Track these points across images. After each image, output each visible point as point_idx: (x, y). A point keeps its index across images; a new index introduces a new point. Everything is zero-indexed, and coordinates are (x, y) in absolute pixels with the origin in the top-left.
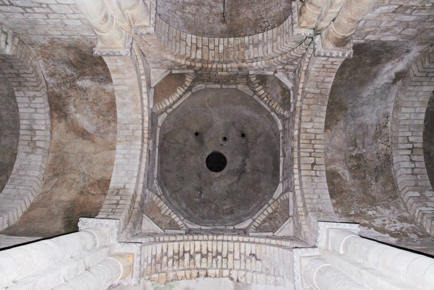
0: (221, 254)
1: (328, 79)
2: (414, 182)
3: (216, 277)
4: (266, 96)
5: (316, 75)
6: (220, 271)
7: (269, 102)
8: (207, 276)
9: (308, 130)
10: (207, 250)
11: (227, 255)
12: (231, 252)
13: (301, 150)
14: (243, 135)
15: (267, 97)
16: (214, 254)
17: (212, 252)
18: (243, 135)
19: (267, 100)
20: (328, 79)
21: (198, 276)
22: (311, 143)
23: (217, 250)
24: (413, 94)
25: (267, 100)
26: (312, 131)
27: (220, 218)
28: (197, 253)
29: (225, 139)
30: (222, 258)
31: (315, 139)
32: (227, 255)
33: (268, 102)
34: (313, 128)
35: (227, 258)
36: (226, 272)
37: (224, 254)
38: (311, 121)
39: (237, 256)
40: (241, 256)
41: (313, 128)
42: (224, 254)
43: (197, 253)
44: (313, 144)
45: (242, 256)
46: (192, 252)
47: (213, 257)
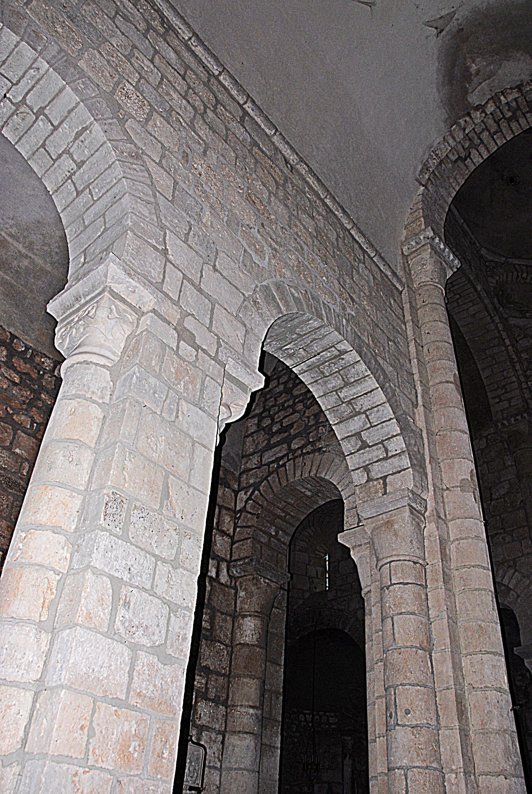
0: (509, 120)
1: (487, 373)
4: (526, 279)
5: (505, 372)
11: (499, 126)
12: (496, 133)
13: (467, 282)
14: (512, 180)
15: (523, 278)
16: (519, 113)
17: (524, 114)
19: (522, 275)
20: (487, 373)
22: (459, 294)
23: (518, 121)
25: (522, 275)
26: (465, 307)
30: (504, 117)
31: (457, 301)
32: (499, 126)
33: (520, 274)
34: (467, 309)
35: (497, 122)
36: (490, 108)
37: (504, 124)
38: (474, 315)
39: (485, 135)
40: (479, 141)
41: (467, 309)
42: (504, 124)
44: (455, 295)
45: (477, 141)
47: (519, 108)
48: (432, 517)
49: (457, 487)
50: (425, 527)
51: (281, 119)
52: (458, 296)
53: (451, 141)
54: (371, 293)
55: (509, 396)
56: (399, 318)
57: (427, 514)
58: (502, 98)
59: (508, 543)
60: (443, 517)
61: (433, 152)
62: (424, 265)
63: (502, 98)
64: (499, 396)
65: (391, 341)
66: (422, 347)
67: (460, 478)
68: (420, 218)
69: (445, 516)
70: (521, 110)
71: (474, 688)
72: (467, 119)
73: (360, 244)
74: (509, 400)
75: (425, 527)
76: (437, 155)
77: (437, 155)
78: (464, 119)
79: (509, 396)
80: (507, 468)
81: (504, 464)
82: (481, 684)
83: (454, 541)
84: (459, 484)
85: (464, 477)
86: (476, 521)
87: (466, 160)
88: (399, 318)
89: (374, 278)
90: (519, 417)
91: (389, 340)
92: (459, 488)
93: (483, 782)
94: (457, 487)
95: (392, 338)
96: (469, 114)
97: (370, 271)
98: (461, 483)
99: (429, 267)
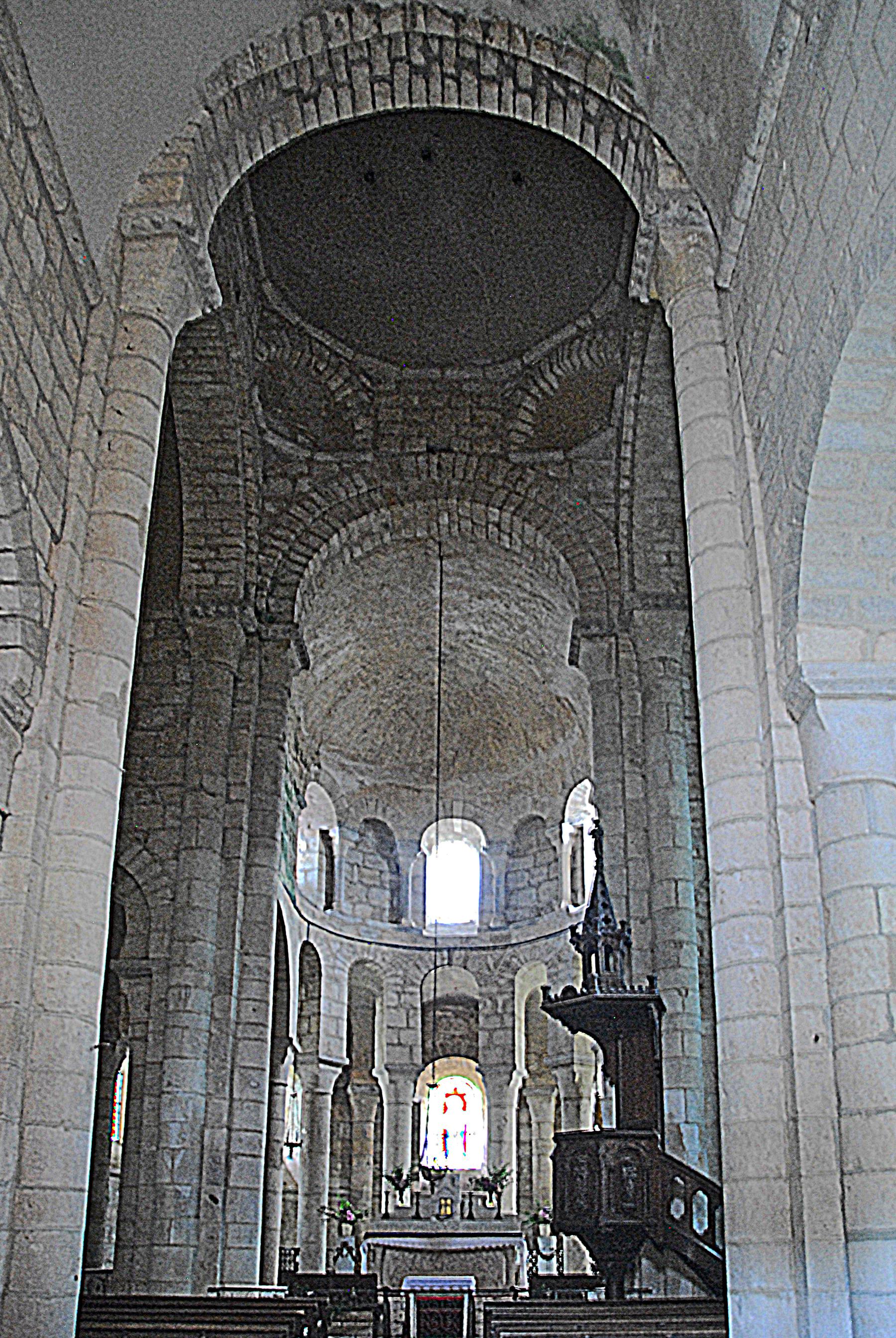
0: (415, 69)
2: (257, 861)
3: (425, 8)
6: (414, 25)
7: (310, 360)
8: (459, 20)
9: (210, 378)
10: (459, 84)
14: (370, 176)
15: (317, 370)
17: (444, 75)
18: (370, 176)
19: (316, 363)
21: (486, 26)
22: (195, 350)
24: (575, 1328)
27: (399, 466)
28: (491, 80)
29: (427, 156)
36: (393, 26)
37: (403, 71)
43: (491, 80)
46: (509, 84)
48: (37, 741)
49: (93, 702)
50: (20, 753)
51: (455, 703)
52: (191, 352)
53: (296, 45)
54: (33, 289)
55: (220, 566)
56: (73, 361)
57: (27, 733)
58: (421, 18)
59: (145, 804)
60: (56, 746)
61: (252, 46)
62: (153, 274)
63: (421, 18)
64: (202, 562)
65: (45, 400)
66: (100, 433)
67: (102, 689)
68: (177, 174)
69: (60, 744)
70: (441, 64)
71: (45, 1010)
72: (344, 19)
73: (40, 170)
74: (218, 574)
75: (20, 753)
76: (258, 58)
77: (258, 58)
78: (337, 14)
79: (220, 566)
80: (177, 685)
81: (175, 677)
82: (59, 1006)
83: (66, 787)
84: (96, 699)
85: (109, 690)
86: (111, 766)
87: (306, 101)
88: (73, 361)
89: (48, 260)
90: (223, 609)
91: (42, 396)
92: (95, 706)
93: (29, 1134)
94: (93, 702)
95: (48, 397)
96: (350, 11)
97: (46, 240)
98: (101, 698)
99: (161, 285)
